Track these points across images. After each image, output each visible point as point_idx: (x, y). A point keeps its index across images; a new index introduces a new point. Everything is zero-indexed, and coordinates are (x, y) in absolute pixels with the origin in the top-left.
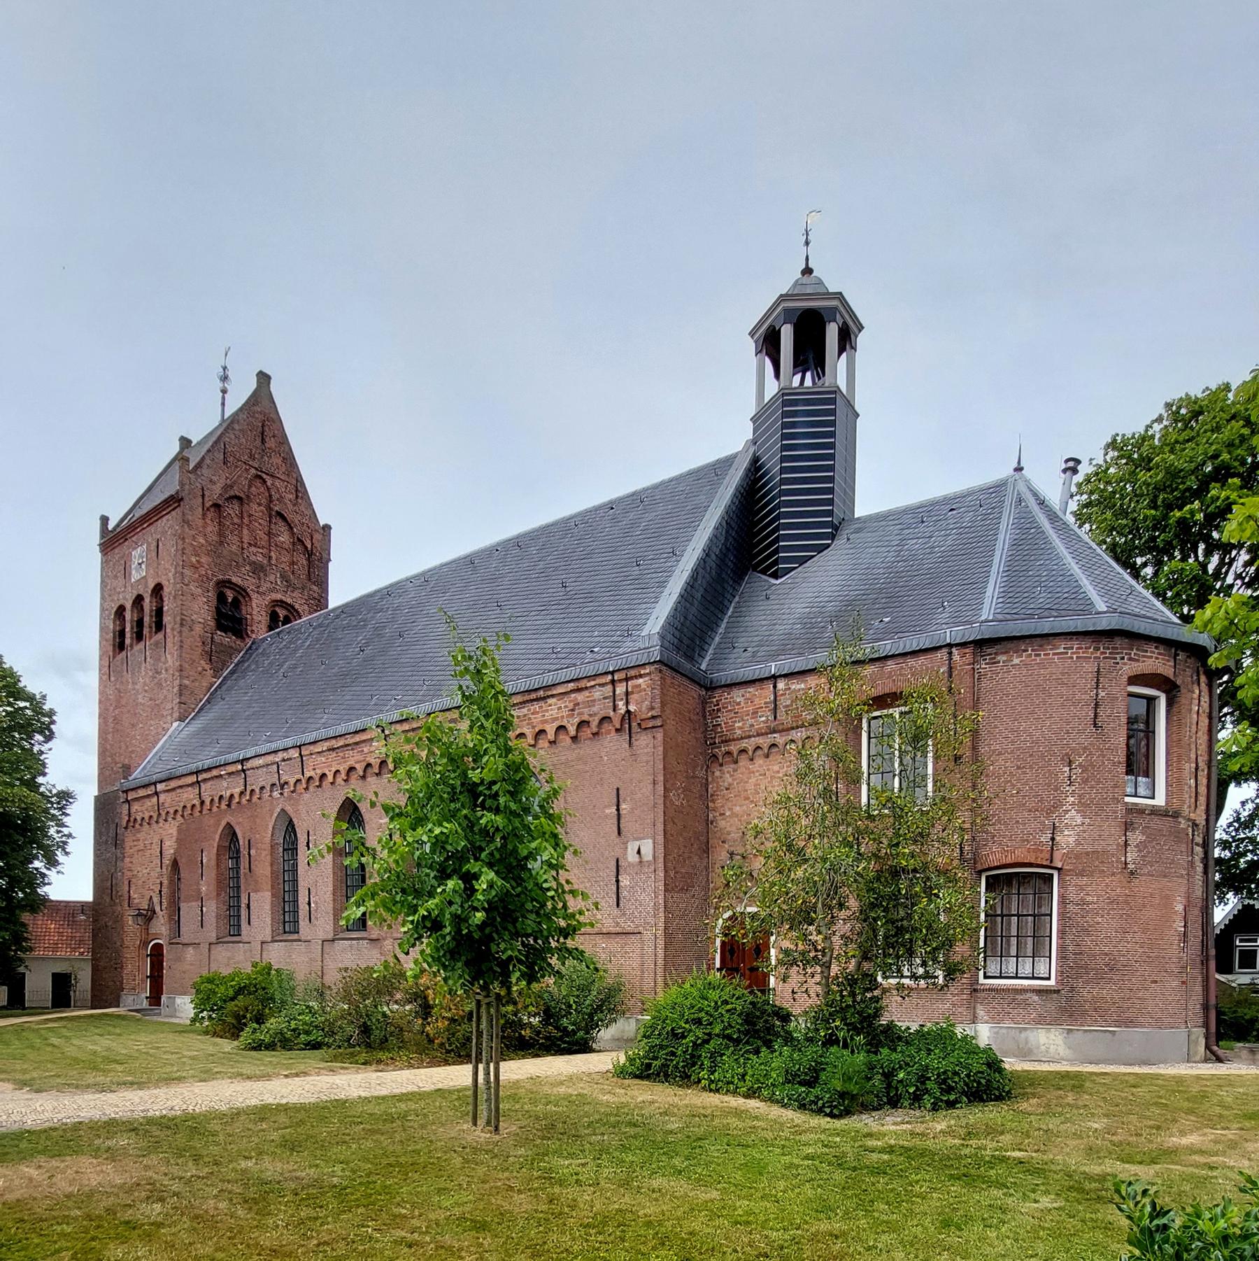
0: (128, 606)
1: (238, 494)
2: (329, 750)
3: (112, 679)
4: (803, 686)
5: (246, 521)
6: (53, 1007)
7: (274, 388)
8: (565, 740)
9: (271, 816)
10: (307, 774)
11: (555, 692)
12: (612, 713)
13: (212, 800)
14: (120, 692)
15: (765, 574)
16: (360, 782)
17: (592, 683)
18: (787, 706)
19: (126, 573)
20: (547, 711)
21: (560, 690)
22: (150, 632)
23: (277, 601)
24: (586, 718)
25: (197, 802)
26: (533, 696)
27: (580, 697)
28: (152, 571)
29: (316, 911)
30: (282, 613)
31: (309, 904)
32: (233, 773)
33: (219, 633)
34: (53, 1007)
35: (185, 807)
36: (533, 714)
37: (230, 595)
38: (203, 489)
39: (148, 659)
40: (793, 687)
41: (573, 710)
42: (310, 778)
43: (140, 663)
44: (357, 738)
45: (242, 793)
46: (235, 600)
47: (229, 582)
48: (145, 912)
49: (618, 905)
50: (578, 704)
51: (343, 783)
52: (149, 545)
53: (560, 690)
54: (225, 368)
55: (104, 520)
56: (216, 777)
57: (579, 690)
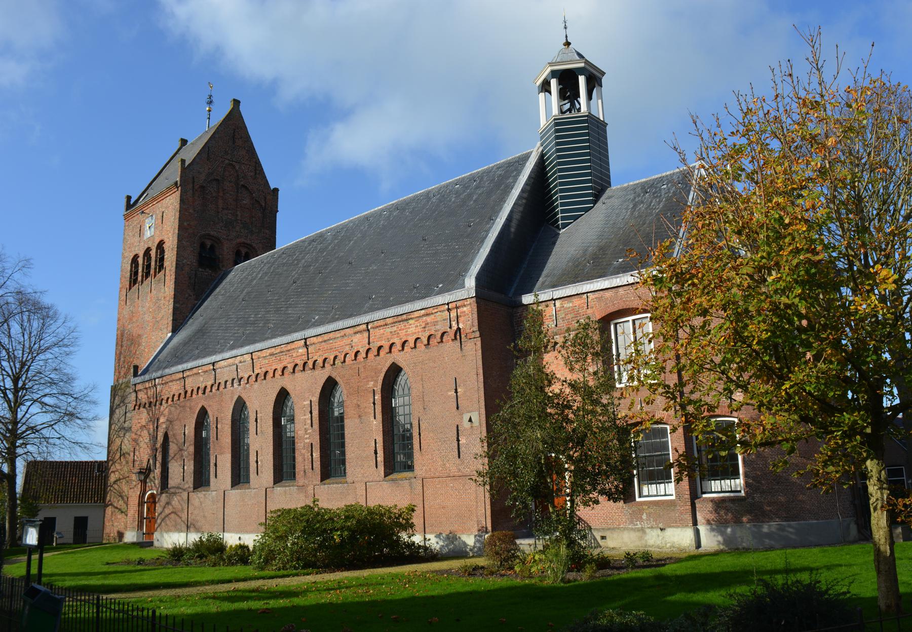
0: (141, 255)
1: (216, 178)
2: (270, 355)
3: (128, 304)
4: (571, 305)
5: (221, 194)
6: (75, 543)
7: (242, 108)
9: (232, 400)
10: (256, 372)
11: (413, 316)
12: (449, 330)
13: (193, 390)
14: (132, 312)
15: (553, 226)
16: (291, 376)
17: (436, 310)
18: (563, 318)
19: (141, 232)
20: (409, 328)
21: (416, 314)
23: (240, 243)
24: (433, 332)
26: (400, 318)
27: (429, 319)
28: (158, 232)
29: (262, 467)
30: (243, 251)
31: (257, 462)
32: (207, 371)
33: (200, 270)
34: (75, 543)
35: (174, 395)
36: (400, 330)
37: (209, 243)
38: (193, 178)
39: (153, 291)
40: (565, 306)
41: (424, 328)
42: (258, 374)
43: (147, 293)
44: (289, 347)
45: (212, 385)
46: (212, 247)
47: (209, 235)
48: (144, 471)
49: (459, 457)
50: (428, 324)
51: (279, 377)
52: (157, 215)
53: (416, 314)
54: (210, 96)
55: (129, 198)
56: (196, 374)
57: (427, 315)
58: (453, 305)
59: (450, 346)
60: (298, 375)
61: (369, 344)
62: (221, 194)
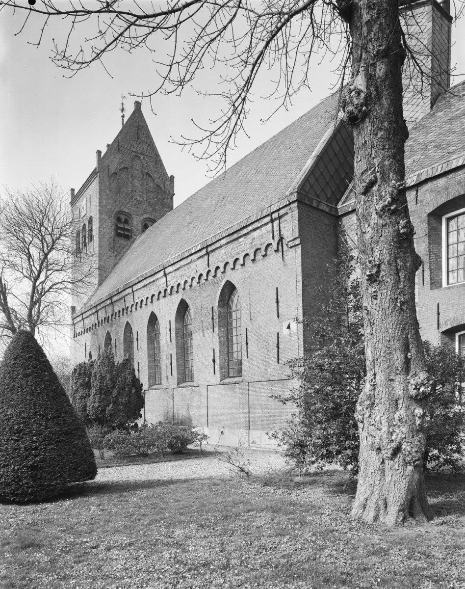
8: (248, 262)
10: (136, 301)
13: (102, 320)
22: (89, 241)
25: (97, 322)
37: (123, 218)
47: (123, 211)
55: (73, 190)
58: (275, 215)
59: (274, 258)
60: (162, 300)
61: (208, 266)
62: (130, 180)
